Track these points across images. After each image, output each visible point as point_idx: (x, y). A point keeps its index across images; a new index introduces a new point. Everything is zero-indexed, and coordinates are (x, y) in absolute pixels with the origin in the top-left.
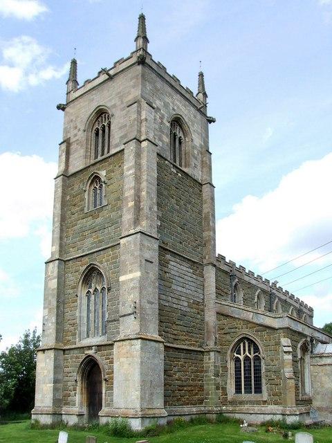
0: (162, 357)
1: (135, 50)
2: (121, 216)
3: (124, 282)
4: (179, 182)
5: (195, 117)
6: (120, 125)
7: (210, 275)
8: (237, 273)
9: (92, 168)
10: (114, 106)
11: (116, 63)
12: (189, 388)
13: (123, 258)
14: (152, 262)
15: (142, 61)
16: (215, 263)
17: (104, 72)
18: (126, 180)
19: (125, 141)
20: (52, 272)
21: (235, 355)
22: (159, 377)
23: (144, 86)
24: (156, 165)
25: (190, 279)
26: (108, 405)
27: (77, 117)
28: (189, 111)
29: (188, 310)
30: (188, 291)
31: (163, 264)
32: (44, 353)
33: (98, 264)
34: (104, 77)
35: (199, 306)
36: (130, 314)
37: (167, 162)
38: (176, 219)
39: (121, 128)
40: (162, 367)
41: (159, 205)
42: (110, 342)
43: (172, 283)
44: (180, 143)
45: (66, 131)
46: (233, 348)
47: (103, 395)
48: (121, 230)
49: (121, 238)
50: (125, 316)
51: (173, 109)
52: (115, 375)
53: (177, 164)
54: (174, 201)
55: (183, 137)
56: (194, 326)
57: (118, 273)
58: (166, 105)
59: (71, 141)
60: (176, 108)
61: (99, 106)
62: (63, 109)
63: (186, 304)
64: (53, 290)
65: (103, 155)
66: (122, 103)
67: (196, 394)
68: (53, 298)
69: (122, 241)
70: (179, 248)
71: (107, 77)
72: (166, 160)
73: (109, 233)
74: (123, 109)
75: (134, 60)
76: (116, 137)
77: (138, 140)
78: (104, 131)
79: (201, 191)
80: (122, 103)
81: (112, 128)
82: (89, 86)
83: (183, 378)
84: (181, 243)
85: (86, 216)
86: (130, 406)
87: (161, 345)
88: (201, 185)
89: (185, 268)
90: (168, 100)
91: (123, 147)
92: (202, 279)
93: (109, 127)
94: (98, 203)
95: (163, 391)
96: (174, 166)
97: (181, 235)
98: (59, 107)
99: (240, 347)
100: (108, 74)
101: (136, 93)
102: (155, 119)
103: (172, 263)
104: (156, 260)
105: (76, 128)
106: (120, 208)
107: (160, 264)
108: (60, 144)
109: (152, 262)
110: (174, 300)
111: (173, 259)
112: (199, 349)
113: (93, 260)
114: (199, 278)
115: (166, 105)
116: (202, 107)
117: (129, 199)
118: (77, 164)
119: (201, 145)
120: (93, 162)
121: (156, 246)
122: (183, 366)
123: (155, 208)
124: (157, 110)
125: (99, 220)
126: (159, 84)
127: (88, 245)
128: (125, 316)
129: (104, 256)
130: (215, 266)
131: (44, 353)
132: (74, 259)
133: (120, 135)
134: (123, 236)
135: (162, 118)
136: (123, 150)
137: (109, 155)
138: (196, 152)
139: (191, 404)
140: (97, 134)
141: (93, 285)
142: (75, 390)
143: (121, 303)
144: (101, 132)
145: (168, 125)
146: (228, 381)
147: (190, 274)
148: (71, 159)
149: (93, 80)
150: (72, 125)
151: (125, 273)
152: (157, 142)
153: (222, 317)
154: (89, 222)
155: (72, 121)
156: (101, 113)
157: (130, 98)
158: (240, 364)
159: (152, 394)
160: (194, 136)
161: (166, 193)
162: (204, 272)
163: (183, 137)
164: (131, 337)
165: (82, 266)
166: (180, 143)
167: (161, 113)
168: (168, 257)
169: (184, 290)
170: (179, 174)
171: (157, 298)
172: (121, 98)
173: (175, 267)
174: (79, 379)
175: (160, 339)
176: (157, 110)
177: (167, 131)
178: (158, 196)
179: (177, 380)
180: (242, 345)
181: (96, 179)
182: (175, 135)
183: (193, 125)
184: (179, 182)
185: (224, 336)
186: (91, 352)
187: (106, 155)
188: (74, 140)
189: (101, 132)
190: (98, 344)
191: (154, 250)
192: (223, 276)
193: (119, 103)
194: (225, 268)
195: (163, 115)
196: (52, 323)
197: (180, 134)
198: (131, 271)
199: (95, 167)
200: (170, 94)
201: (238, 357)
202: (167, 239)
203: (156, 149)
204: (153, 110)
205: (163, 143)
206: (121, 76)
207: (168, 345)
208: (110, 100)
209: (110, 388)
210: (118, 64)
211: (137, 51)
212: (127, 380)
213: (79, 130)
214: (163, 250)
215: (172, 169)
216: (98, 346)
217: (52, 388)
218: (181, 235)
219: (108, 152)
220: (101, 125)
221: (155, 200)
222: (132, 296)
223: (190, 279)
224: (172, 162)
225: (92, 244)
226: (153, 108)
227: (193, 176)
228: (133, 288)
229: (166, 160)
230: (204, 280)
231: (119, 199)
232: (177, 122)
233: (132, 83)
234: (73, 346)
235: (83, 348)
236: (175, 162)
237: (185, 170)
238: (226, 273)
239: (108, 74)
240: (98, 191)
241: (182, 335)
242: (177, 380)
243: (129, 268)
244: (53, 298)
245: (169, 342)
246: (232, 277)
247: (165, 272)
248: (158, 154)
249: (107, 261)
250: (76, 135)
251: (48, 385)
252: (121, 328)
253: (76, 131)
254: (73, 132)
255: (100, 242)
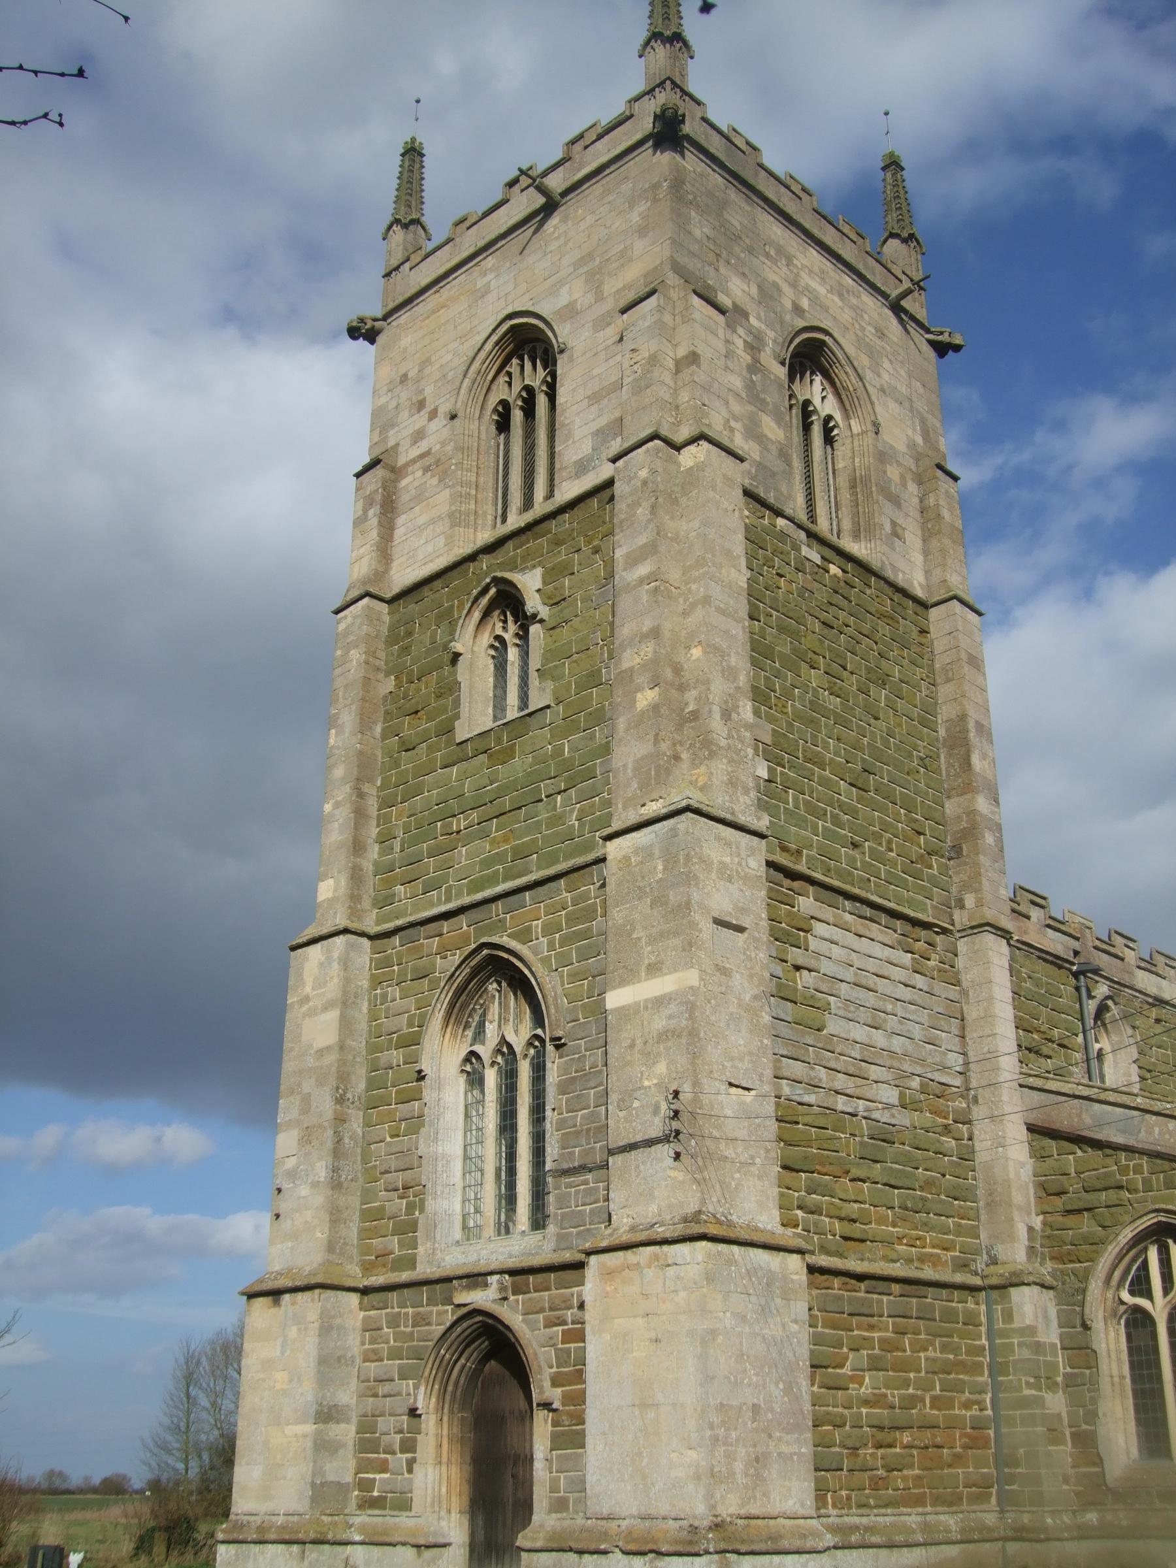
0: (800, 1307)
1: (640, 86)
2: (606, 749)
3: (626, 1013)
4: (837, 599)
5: (881, 334)
6: (594, 386)
7: (991, 969)
8: (1102, 960)
9: (485, 562)
10: (570, 312)
11: (573, 142)
12: (927, 1436)
13: (617, 915)
14: (740, 929)
15: (669, 133)
16: (1007, 923)
17: (525, 182)
18: (625, 604)
19: (616, 446)
20: (319, 983)
21: (1125, 1296)
22: (788, 1390)
23: (682, 226)
24: (740, 537)
25: (906, 994)
26: (560, 1505)
27: (426, 362)
28: (858, 311)
29: (903, 1118)
30: (897, 1044)
31: (788, 933)
32: (277, 1303)
33: (513, 944)
34: (526, 202)
35: (947, 1109)
36: (650, 1143)
37: (781, 522)
38: (831, 751)
39: (595, 398)
40: (802, 1350)
41: (759, 696)
42: (567, 1256)
43: (826, 1008)
44: (829, 440)
45: (382, 421)
46: (1120, 1257)
47: (539, 1466)
48: (608, 803)
49: (609, 838)
50: (633, 1147)
51: (798, 310)
52: (594, 1386)
53: (823, 525)
54: (815, 678)
55: (838, 416)
56: (928, 1185)
57: (597, 980)
58: (767, 294)
59: (401, 461)
60: (805, 303)
61: (510, 316)
62: (371, 336)
63: (891, 1095)
64: (321, 1052)
65: (528, 503)
66: (599, 298)
67: (958, 1460)
68: (320, 1083)
69: (613, 849)
70: (849, 865)
71: (541, 200)
72: (779, 513)
73: (557, 819)
74: (601, 323)
75: (645, 124)
76: (577, 434)
77: (666, 441)
78: (529, 411)
79: (924, 632)
80: (599, 298)
81: (561, 399)
82: (470, 241)
83: (894, 1396)
84: (855, 845)
85: (463, 752)
86: (664, 1508)
87: (794, 1261)
88: (924, 605)
89: (878, 948)
90: (775, 274)
91: (606, 471)
92: (952, 992)
93: (552, 397)
94: (513, 697)
95: (807, 1450)
96: (811, 535)
97: (853, 812)
98: (354, 332)
99: (1145, 1265)
100: (542, 190)
101: (647, 256)
102: (728, 355)
103: (819, 928)
104: (757, 918)
105: (421, 405)
106: (600, 718)
107: (777, 936)
108: (358, 475)
109: (740, 929)
110: (841, 1082)
111: (827, 913)
112: (959, 1278)
113: (490, 930)
114: (940, 988)
115: (767, 294)
116: (908, 292)
117: (640, 679)
118: (422, 550)
119: (912, 446)
120: (485, 536)
121: (756, 865)
122: (888, 1346)
123: (746, 710)
124: (732, 314)
125: (520, 764)
126: (740, 212)
127: (467, 867)
128: (633, 1147)
129: (536, 912)
130: (1005, 934)
131: (277, 1303)
132: (412, 925)
133: (595, 426)
134: (616, 826)
135: (754, 348)
136: (610, 483)
137: (550, 507)
138: (893, 473)
139: (937, 1500)
140: (503, 425)
141: (491, 1029)
142: (409, 1446)
143: (614, 1097)
144: (517, 416)
145: (782, 372)
146: (1104, 1407)
147: (897, 973)
148: (399, 532)
149: (486, 214)
150: (405, 395)
151: (630, 977)
152: (739, 443)
153: (1052, 1145)
154: (466, 778)
155: (404, 378)
156: (527, 341)
157: (632, 276)
158: (1154, 1336)
159: (759, 1460)
160: (887, 411)
161: (784, 647)
162: (960, 962)
163: (838, 416)
164: (661, 1231)
165: (442, 952)
166: (829, 440)
167: (750, 331)
168: (807, 903)
169: (879, 1039)
170: (834, 569)
171: (769, 1073)
172: (594, 281)
173: (841, 945)
174: (424, 1400)
175: (789, 1236)
176: (732, 314)
177: (775, 397)
178: (755, 663)
179: (866, 1402)
180: (1153, 1255)
181: (508, 600)
182: (806, 411)
183: (876, 368)
184: (837, 599)
185: (1071, 1220)
186: (482, 1298)
187: (540, 507)
188: (415, 452)
189: (517, 416)
190: (512, 1263)
191: (746, 878)
192: (1043, 971)
193: (590, 298)
194: (1055, 943)
195: (758, 337)
196: (315, 1185)
197: (826, 406)
198: (654, 969)
199: (499, 557)
200: (780, 251)
201: (1137, 1309)
202: (795, 834)
203: (739, 474)
204: (721, 318)
205: (765, 448)
206: (594, 190)
207: (823, 1261)
208: (553, 291)
209: (571, 1438)
210: (578, 147)
211: (650, 92)
212: (645, 1405)
213: (433, 414)
214: (782, 872)
215: (805, 551)
216: (513, 1272)
217: (309, 1443)
218: (853, 812)
219: (550, 494)
220: (517, 387)
221: (743, 680)
222: (661, 1068)
223: (906, 994)
224: (802, 517)
225: (487, 863)
226: (722, 312)
227: (889, 574)
228: (664, 1036)
229: (779, 513)
230: (965, 993)
231: (593, 679)
232: (810, 356)
233: (635, 217)
234: (405, 1276)
235: (448, 1280)
236: (812, 517)
237: (857, 549)
238: (1056, 961)
239: (542, 190)
240: (513, 654)
241: (882, 1220)
242: (866, 1402)
243: (648, 955)
244: (320, 1083)
245: (824, 1250)
246: (1084, 973)
247: (798, 968)
248: (747, 493)
249: (548, 930)
250: (419, 436)
251: (291, 1430)
252: (617, 1196)
253: (420, 420)
254: (411, 422)
255: (521, 854)
